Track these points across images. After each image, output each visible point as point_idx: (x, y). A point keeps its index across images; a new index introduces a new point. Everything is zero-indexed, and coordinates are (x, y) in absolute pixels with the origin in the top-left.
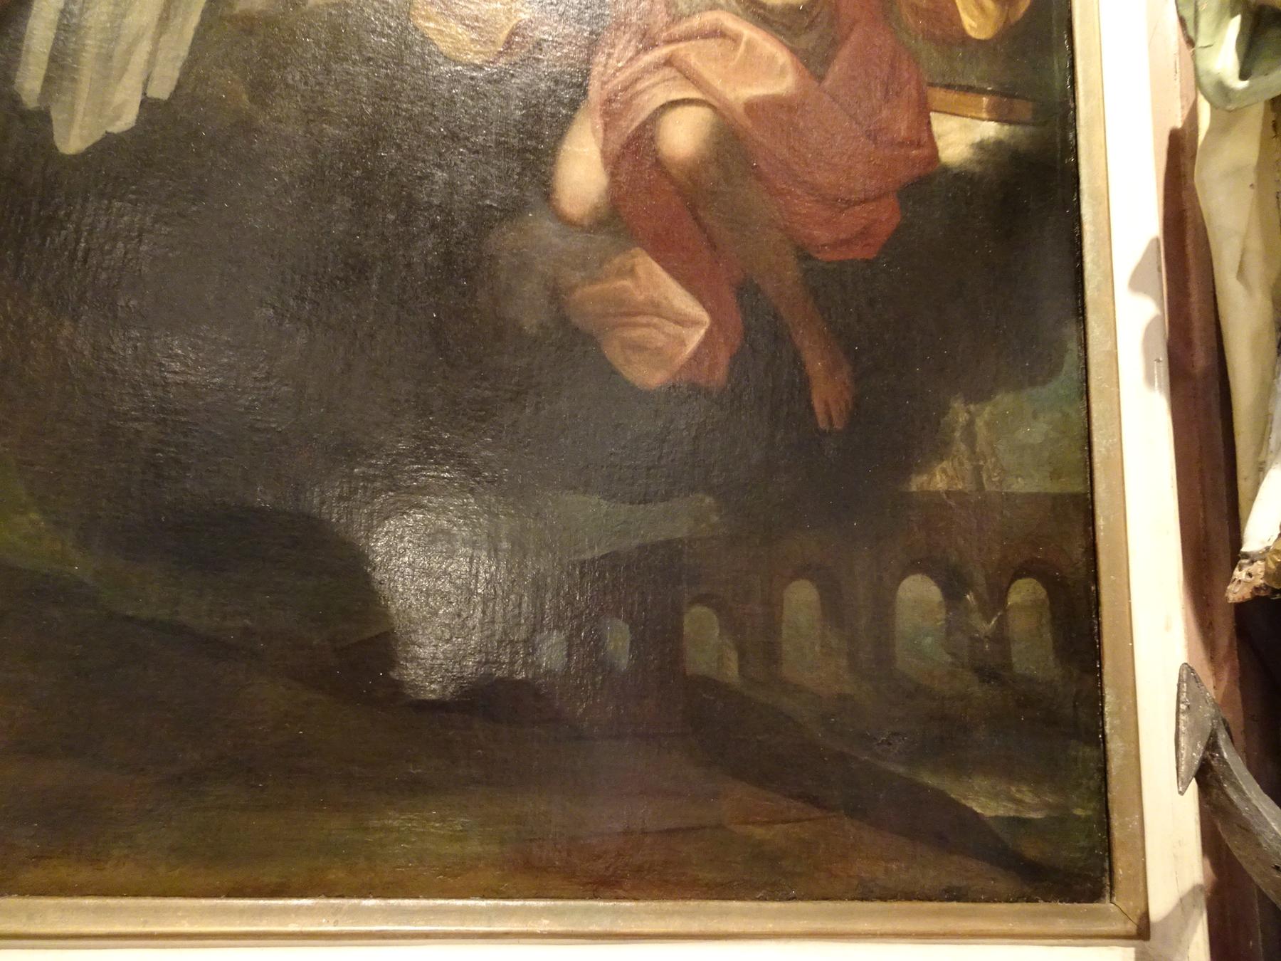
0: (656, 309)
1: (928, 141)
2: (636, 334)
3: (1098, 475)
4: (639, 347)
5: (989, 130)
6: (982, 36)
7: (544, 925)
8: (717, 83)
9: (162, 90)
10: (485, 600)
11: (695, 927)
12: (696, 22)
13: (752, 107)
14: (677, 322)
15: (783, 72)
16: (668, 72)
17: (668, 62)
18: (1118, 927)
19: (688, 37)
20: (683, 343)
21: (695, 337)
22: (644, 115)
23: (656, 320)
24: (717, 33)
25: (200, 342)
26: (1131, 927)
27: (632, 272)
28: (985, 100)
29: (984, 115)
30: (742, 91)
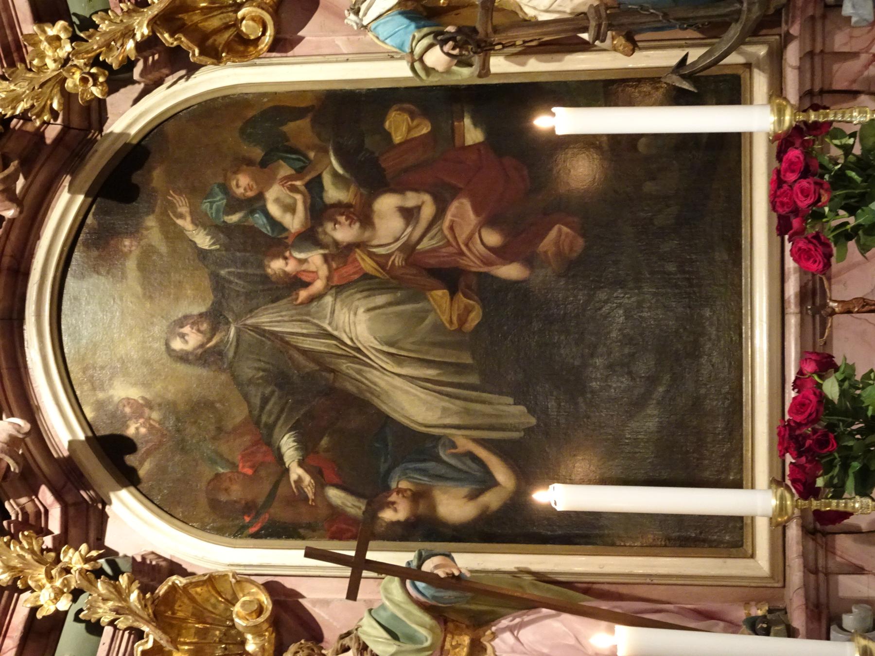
0: (557, 243)
1: (476, 146)
2: (567, 248)
3: (596, 78)
4: (571, 250)
5: (467, 121)
6: (429, 124)
7: (748, 186)
8: (472, 227)
9: (511, 400)
10: (657, 289)
11: (748, 152)
12: (449, 237)
13: (477, 212)
14: (560, 236)
15: (462, 203)
16: (470, 245)
17: (467, 245)
18: (748, 75)
19: (455, 238)
20: (567, 234)
21: (565, 229)
22: (489, 252)
23: (561, 242)
24: (451, 228)
25: (640, 244)
26: (748, 70)
27: (546, 252)
28: (456, 123)
29: (462, 123)
30: (472, 219)
